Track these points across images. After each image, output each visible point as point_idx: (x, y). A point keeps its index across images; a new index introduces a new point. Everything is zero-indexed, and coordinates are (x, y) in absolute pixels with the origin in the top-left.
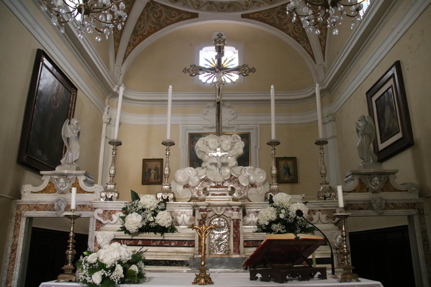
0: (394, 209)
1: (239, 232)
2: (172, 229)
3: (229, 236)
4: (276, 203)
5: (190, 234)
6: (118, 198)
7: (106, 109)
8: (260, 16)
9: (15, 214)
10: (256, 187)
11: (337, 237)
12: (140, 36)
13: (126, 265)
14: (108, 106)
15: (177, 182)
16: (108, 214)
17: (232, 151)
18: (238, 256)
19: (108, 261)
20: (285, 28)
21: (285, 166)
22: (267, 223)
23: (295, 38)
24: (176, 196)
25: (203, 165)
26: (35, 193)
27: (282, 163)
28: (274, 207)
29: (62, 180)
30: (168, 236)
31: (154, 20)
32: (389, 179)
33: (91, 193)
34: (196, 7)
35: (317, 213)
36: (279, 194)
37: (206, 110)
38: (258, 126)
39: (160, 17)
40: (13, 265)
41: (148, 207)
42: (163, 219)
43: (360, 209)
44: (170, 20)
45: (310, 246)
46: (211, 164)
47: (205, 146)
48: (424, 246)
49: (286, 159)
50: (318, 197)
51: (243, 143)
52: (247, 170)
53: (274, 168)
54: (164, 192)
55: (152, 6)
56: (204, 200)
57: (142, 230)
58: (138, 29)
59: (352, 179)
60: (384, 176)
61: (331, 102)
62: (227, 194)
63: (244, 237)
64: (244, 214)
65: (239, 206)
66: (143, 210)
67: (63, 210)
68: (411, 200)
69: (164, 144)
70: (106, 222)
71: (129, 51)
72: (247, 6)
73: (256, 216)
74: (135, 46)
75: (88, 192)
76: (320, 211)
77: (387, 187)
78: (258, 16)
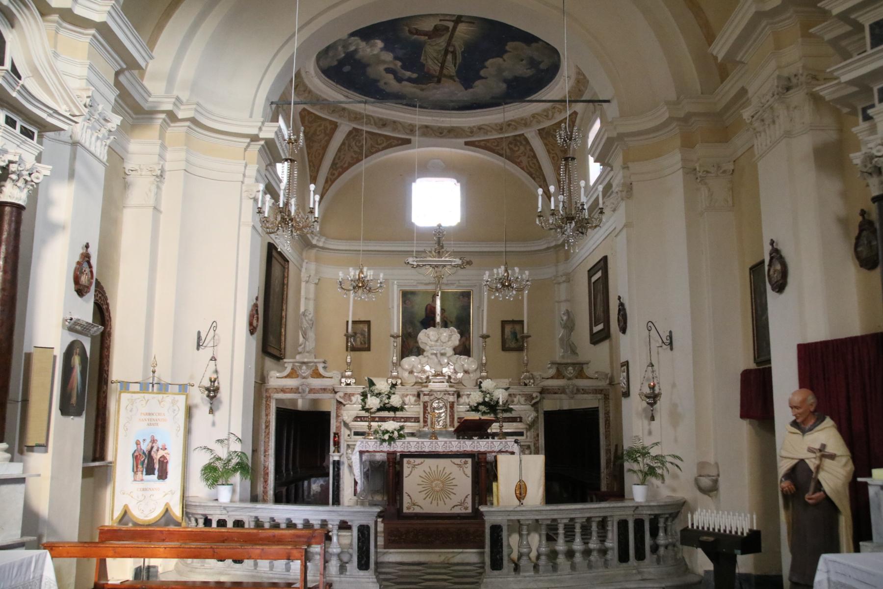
2: (402, 409)
7: (304, 264)
8: (488, 144)
13: (399, 431)
16: (348, 396)
25: (425, 354)
27: (508, 329)
29: (304, 367)
30: (399, 414)
31: (357, 149)
34: (408, 131)
42: (395, 401)
43: (555, 393)
46: (432, 354)
49: (513, 322)
54: (393, 378)
55: (354, 133)
56: (427, 386)
57: (379, 410)
64: (459, 396)
66: (380, 394)
74: (333, 181)
77: (581, 375)
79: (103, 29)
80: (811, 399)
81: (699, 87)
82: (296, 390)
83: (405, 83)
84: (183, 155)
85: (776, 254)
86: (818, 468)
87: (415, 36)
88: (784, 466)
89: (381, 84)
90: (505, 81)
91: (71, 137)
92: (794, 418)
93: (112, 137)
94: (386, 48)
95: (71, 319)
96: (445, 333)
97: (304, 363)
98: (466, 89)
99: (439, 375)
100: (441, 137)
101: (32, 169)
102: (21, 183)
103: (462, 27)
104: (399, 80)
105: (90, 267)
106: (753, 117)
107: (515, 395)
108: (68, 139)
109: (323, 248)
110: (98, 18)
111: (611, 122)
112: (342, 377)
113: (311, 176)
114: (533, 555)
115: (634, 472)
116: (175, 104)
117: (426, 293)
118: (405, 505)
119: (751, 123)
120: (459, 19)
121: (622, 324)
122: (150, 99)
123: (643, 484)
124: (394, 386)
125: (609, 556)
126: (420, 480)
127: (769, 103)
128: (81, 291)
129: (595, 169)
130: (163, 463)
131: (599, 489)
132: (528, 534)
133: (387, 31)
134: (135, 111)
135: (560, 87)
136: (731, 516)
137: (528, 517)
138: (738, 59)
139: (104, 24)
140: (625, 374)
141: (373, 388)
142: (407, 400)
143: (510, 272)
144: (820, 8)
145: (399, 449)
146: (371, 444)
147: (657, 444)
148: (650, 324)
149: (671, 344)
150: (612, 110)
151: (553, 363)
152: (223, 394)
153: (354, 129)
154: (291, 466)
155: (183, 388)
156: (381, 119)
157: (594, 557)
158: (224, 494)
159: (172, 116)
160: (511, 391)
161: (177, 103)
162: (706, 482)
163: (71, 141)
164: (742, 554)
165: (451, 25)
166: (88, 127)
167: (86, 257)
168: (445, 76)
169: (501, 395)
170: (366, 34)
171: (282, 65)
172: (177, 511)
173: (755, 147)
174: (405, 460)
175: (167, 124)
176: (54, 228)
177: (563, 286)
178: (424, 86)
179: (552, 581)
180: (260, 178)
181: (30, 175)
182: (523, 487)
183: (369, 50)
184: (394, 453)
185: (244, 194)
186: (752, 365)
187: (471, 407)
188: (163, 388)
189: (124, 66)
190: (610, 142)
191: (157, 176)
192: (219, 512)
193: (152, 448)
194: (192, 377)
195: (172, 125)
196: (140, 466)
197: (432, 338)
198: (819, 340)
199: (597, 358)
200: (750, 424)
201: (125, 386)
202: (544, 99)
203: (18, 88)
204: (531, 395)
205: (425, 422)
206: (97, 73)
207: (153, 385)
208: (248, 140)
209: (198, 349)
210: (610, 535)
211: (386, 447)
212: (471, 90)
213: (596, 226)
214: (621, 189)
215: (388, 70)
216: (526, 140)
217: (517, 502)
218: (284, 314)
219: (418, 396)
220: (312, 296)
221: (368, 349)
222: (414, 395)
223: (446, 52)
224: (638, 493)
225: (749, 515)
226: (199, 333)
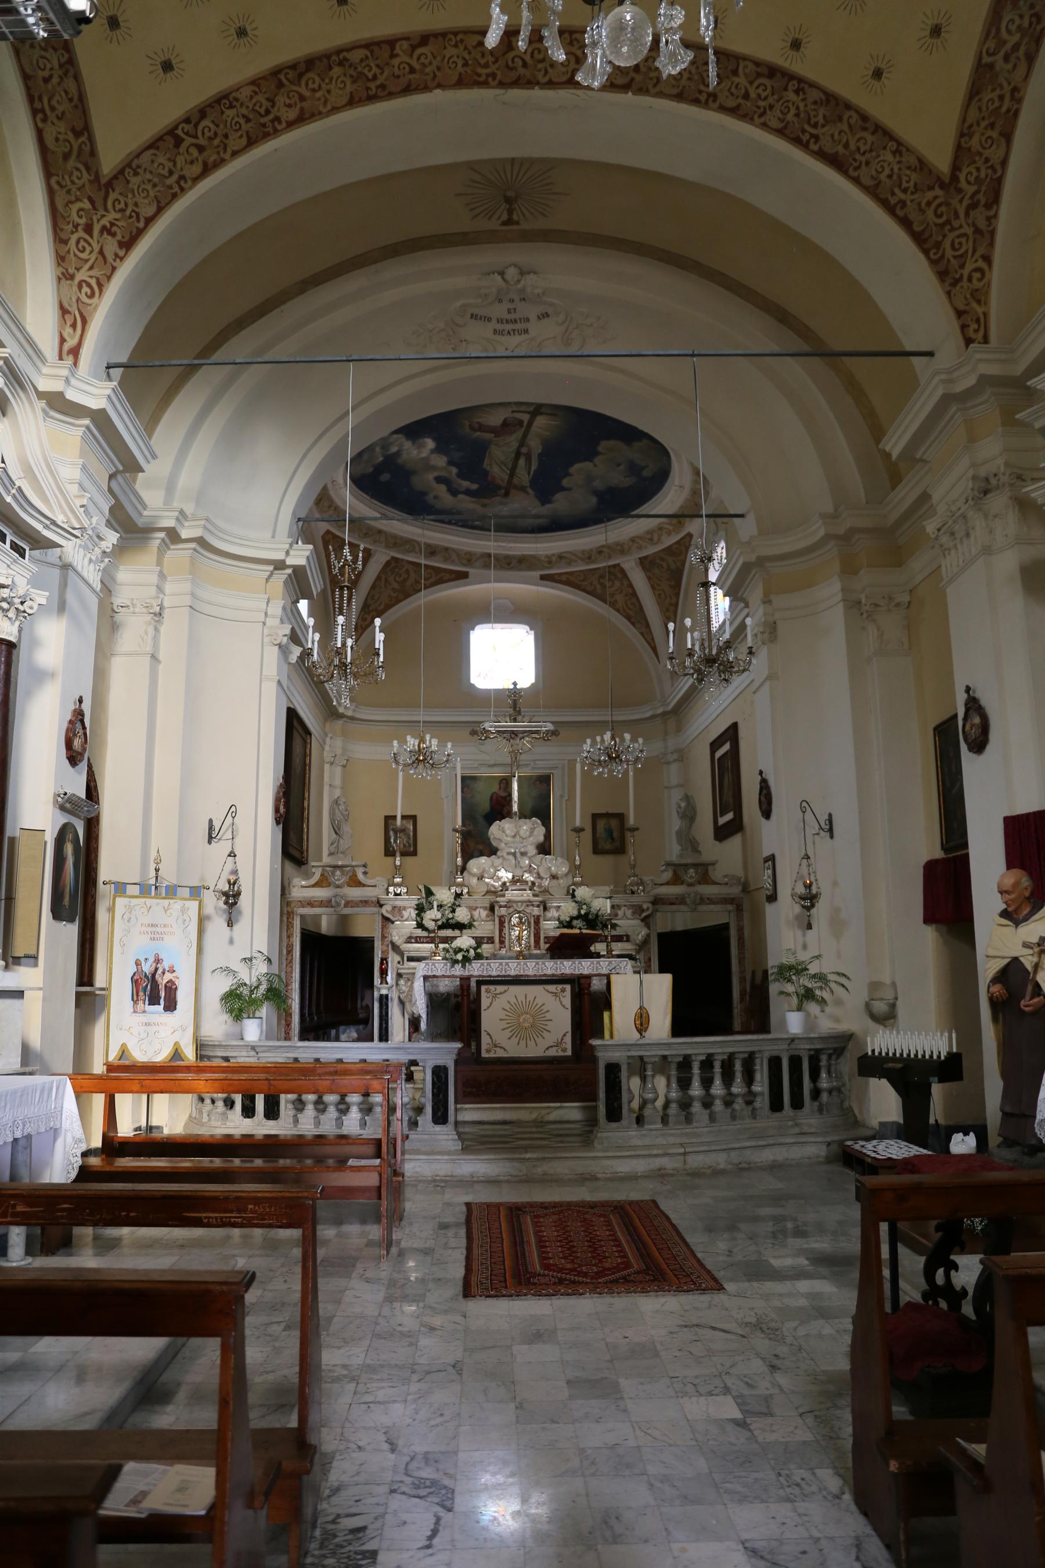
2: (470, 926)
3: (529, 932)
7: (328, 740)
14: (330, 735)
16: (398, 910)
17: (531, 839)
19: (464, 946)
23: (628, 618)
25: (498, 853)
29: (338, 873)
31: (396, 586)
39: (405, 580)
42: (462, 915)
43: (672, 904)
46: (509, 853)
49: (608, 815)
53: (577, 858)
56: (504, 896)
59: (665, 870)
61: (679, 729)
64: (545, 909)
77: (705, 878)
79: (100, 419)
80: (1026, 882)
81: (863, 495)
82: (322, 904)
84: (187, 586)
85: (973, 705)
86: (1036, 967)
87: (478, 433)
88: (988, 969)
90: (596, 493)
91: (60, 557)
92: (1004, 906)
93: (107, 560)
94: (438, 450)
95: (65, 794)
97: (336, 867)
98: (543, 504)
99: (518, 881)
101: (25, 596)
102: (12, 614)
103: (540, 421)
104: (454, 492)
105: (84, 728)
106: (939, 530)
107: (619, 907)
108: (57, 561)
109: (352, 718)
110: (94, 404)
111: (749, 543)
114: (660, 1103)
115: (788, 995)
116: (177, 519)
119: (936, 538)
120: (537, 410)
121: (765, 806)
122: (145, 513)
123: (799, 1009)
124: (458, 896)
125: (758, 1104)
127: (961, 511)
128: (73, 759)
129: (720, 604)
130: (171, 990)
132: (653, 1076)
133: (440, 427)
134: (130, 529)
135: (669, 500)
136: (924, 1038)
137: (653, 1053)
138: (918, 457)
139: (103, 412)
140: (770, 872)
141: (432, 898)
142: (476, 914)
143: (617, 740)
144: (1029, 388)
145: (476, 973)
146: (439, 966)
147: (818, 957)
148: (804, 804)
149: (831, 830)
150: (747, 528)
151: (668, 864)
152: (244, 901)
153: (393, 558)
155: (196, 892)
157: (739, 1105)
158: (252, 1030)
159: (173, 536)
160: (617, 901)
161: (181, 518)
162: (880, 1007)
163: (60, 564)
164: (940, 1081)
165: (525, 418)
166: (80, 546)
167: (79, 714)
168: (515, 487)
169: (602, 905)
170: (413, 431)
171: (314, 468)
172: (189, 1054)
173: (943, 569)
174: (483, 988)
175: (166, 545)
176: (41, 676)
177: (674, 768)
178: (486, 501)
180: (285, 619)
181: (22, 603)
182: (644, 1015)
183: (415, 452)
185: (266, 640)
186: (938, 854)
187: (561, 922)
188: (172, 892)
189: (121, 468)
190: (746, 569)
191: (155, 614)
192: (244, 1054)
193: (156, 969)
194: (202, 879)
195: (172, 547)
196: (141, 994)
197: (508, 832)
198: (1031, 811)
199: (727, 858)
200: (937, 930)
201: (120, 888)
202: (653, 513)
203: (14, 491)
204: (640, 907)
205: (502, 942)
206: (90, 476)
207: (154, 888)
208: (271, 568)
209: (210, 842)
210: (758, 1076)
211: (458, 970)
213: (744, 671)
214: (761, 630)
215: (439, 480)
216: (623, 572)
218: (306, 805)
219: (492, 909)
220: (338, 782)
222: (485, 908)
223: (518, 454)
224: (794, 1023)
225: (946, 1034)
226: (211, 821)
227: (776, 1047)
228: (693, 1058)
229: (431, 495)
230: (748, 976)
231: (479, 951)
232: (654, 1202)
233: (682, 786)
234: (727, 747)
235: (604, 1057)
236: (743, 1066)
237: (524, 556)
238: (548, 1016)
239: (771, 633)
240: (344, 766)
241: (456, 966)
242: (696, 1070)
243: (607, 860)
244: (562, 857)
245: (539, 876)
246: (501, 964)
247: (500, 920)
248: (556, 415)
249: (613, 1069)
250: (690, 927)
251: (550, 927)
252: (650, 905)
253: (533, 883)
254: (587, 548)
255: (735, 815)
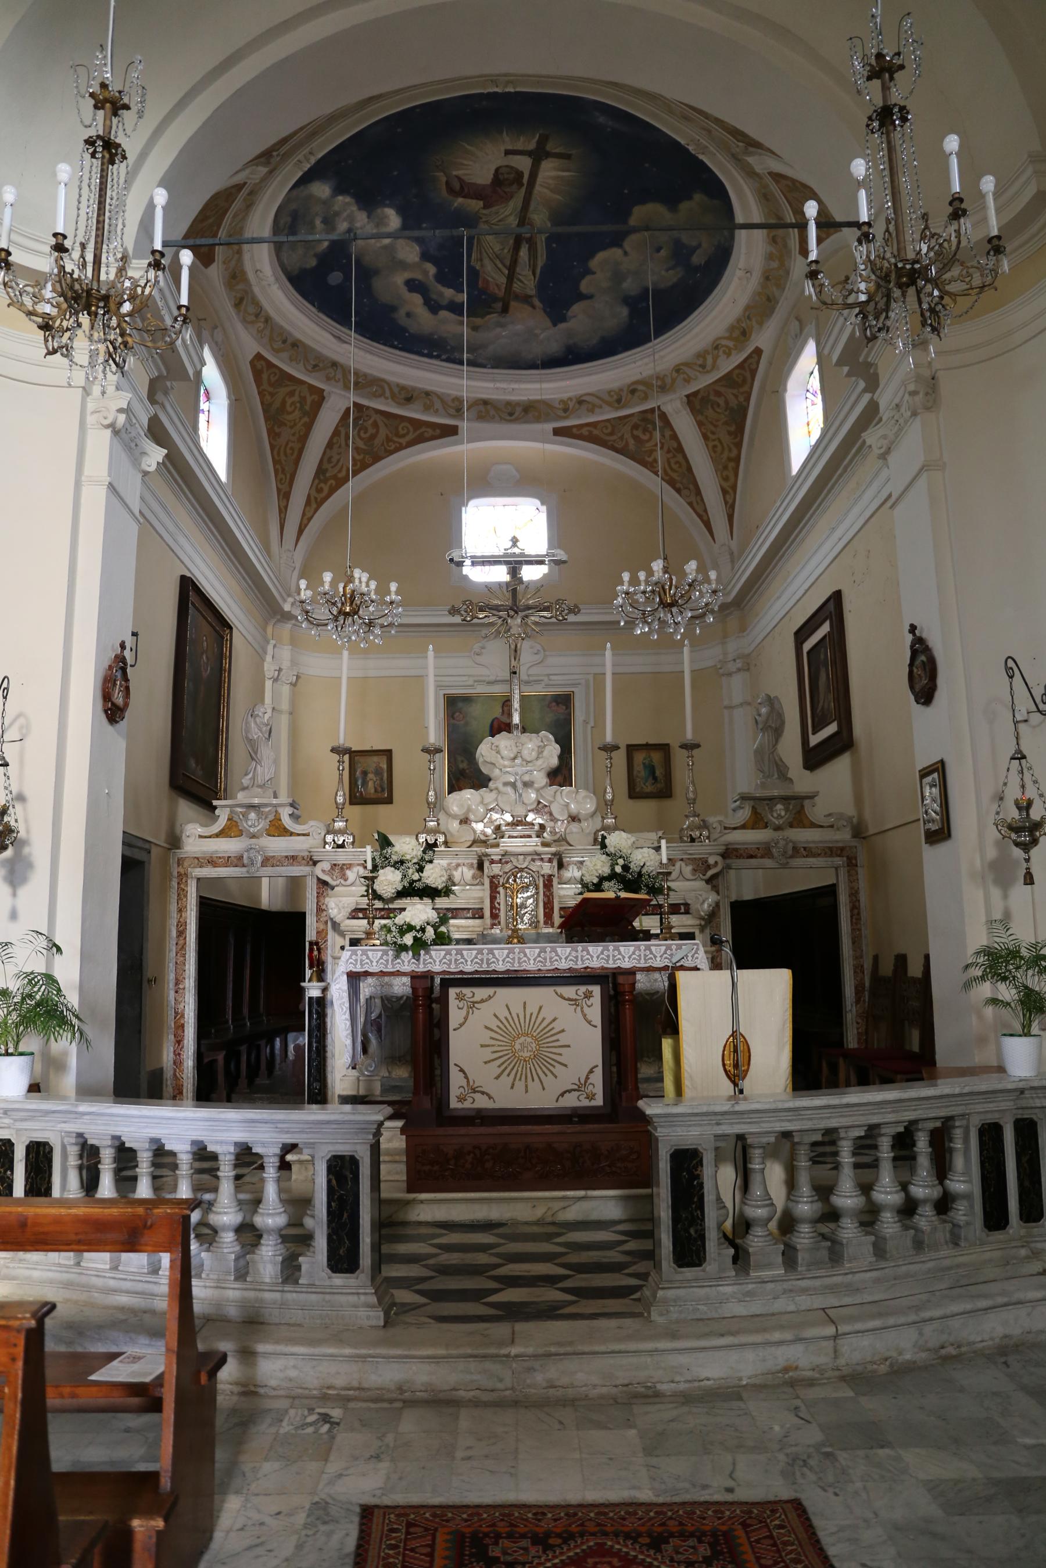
0: (807, 856)
1: (552, 894)
2: (447, 892)
3: (537, 900)
4: (611, 849)
5: (475, 898)
6: (353, 843)
7: (270, 648)
8: (596, 432)
9: (175, 874)
10: (579, 820)
11: (704, 901)
12: (333, 482)
14: (273, 642)
15: (448, 814)
16: (340, 869)
17: (540, 762)
18: (551, 930)
19: (417, 922)
20: (650, 459)
21: (647, 762)
22: (596, 880)
23: (671, 483)
24: (449, 839)
25: (491, 784)
26: (206, 837)
27: (639, 757)
28: (608, 855)
29: (253, 815)
32: (802, 806)
33: (304, 835)
34: (452, 412)
35: (678, 864)
36: (617, 832)
37: (480, 644)
38: (591, 678)
39: (373, 437)
40: (184, 956)
41: (408, 857)
42: (433, 875)
43: (751, 857)
44: (394, 442)
45: (634, 906)
46: (506, 784)
47: (494, 752)
48: (852, 917)
49: (647, 747)
50: (681, 838)
51: (558, 746)
52: (564, 793)
53: (609, 790)
54: (430, 831)
56: (497, 845)
58: (326, 466)
59: (740, 807)
60: (793, 802)
61: (743, 628)
62: (534, 836)
63: (560, 902)
64: (561, 866)
65: (552, 854)
66: (402, 862)
67: (259, 865)
68: (837, 841)
69: (425, 750)
70: (338, 882)
71: (308, 515)
72: (565, 410)
73: (579, 869)
74: (320, 503)
75: (299, 835)
76: (682, 860)
77: (799, 820)
78: (591, 432)
83: (444, 314)
87: (460, 200)
89: (400, 316)
90: (628, 301)
96: (530, 744)
97: (252, 807)
100: (510, 421)
104: (433, 307)
112: (328, 832)
113: (279, 490)
117: (491, 698)
118: (454, 1091)
125: (960, 1212)
126: (485, 1037)
131: (840, 1043)
142: (457, 875)
145: (437, 968)
146: (374, 958)
148: (1010, 661)
151: (744, 798)
154: (246, 1011)
156: (403, 388)
157: (925, 1218)
168: (516, 297)
174: (453, 992)
179: (832, 1289)
182: (740, 1048)
184: (429, 976)
185: (90, 419)
197: (505, 753)
205: (494, 916)
210: (958, 1162)
212: (562, 326)
216: (664, 417)
217: (727, 1087)
219: (480, 866)
220: (285, 706)
221: (389, 801)
227: (991, 1106)
228: (842, 1135)
229: (402, 312)
230: (868, 964)
231: (443, 929)
232: (797, 1505)
233: (749, 704)
234: (825, 628)
235: (669, 1138)
236: (931, 1144)
237: (530, 401)
238: (563, 1039)
239: (927, 394)
240: (294, 685)
241: (403, 955)
242: (846, 1158)
243: (647, 807)
244: (587, 789)
245: (554, 819)
246: (480, 951)
247: (491, 882)
248: (568, 157)
249: (686, 1162)
250: (763, 895)
251: (568, 894)
252: (719, 859)
253: (542, 827)
254: (615, 385)
255: (839, 726)
